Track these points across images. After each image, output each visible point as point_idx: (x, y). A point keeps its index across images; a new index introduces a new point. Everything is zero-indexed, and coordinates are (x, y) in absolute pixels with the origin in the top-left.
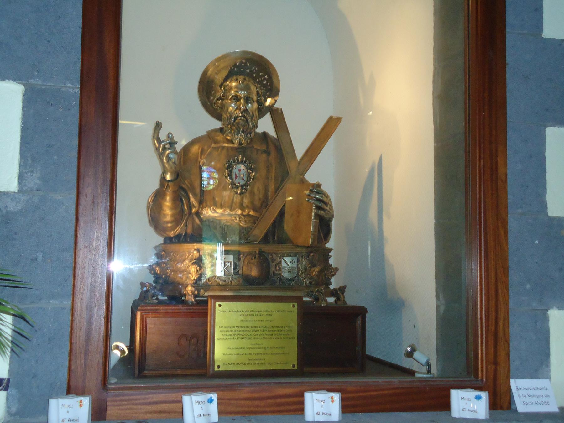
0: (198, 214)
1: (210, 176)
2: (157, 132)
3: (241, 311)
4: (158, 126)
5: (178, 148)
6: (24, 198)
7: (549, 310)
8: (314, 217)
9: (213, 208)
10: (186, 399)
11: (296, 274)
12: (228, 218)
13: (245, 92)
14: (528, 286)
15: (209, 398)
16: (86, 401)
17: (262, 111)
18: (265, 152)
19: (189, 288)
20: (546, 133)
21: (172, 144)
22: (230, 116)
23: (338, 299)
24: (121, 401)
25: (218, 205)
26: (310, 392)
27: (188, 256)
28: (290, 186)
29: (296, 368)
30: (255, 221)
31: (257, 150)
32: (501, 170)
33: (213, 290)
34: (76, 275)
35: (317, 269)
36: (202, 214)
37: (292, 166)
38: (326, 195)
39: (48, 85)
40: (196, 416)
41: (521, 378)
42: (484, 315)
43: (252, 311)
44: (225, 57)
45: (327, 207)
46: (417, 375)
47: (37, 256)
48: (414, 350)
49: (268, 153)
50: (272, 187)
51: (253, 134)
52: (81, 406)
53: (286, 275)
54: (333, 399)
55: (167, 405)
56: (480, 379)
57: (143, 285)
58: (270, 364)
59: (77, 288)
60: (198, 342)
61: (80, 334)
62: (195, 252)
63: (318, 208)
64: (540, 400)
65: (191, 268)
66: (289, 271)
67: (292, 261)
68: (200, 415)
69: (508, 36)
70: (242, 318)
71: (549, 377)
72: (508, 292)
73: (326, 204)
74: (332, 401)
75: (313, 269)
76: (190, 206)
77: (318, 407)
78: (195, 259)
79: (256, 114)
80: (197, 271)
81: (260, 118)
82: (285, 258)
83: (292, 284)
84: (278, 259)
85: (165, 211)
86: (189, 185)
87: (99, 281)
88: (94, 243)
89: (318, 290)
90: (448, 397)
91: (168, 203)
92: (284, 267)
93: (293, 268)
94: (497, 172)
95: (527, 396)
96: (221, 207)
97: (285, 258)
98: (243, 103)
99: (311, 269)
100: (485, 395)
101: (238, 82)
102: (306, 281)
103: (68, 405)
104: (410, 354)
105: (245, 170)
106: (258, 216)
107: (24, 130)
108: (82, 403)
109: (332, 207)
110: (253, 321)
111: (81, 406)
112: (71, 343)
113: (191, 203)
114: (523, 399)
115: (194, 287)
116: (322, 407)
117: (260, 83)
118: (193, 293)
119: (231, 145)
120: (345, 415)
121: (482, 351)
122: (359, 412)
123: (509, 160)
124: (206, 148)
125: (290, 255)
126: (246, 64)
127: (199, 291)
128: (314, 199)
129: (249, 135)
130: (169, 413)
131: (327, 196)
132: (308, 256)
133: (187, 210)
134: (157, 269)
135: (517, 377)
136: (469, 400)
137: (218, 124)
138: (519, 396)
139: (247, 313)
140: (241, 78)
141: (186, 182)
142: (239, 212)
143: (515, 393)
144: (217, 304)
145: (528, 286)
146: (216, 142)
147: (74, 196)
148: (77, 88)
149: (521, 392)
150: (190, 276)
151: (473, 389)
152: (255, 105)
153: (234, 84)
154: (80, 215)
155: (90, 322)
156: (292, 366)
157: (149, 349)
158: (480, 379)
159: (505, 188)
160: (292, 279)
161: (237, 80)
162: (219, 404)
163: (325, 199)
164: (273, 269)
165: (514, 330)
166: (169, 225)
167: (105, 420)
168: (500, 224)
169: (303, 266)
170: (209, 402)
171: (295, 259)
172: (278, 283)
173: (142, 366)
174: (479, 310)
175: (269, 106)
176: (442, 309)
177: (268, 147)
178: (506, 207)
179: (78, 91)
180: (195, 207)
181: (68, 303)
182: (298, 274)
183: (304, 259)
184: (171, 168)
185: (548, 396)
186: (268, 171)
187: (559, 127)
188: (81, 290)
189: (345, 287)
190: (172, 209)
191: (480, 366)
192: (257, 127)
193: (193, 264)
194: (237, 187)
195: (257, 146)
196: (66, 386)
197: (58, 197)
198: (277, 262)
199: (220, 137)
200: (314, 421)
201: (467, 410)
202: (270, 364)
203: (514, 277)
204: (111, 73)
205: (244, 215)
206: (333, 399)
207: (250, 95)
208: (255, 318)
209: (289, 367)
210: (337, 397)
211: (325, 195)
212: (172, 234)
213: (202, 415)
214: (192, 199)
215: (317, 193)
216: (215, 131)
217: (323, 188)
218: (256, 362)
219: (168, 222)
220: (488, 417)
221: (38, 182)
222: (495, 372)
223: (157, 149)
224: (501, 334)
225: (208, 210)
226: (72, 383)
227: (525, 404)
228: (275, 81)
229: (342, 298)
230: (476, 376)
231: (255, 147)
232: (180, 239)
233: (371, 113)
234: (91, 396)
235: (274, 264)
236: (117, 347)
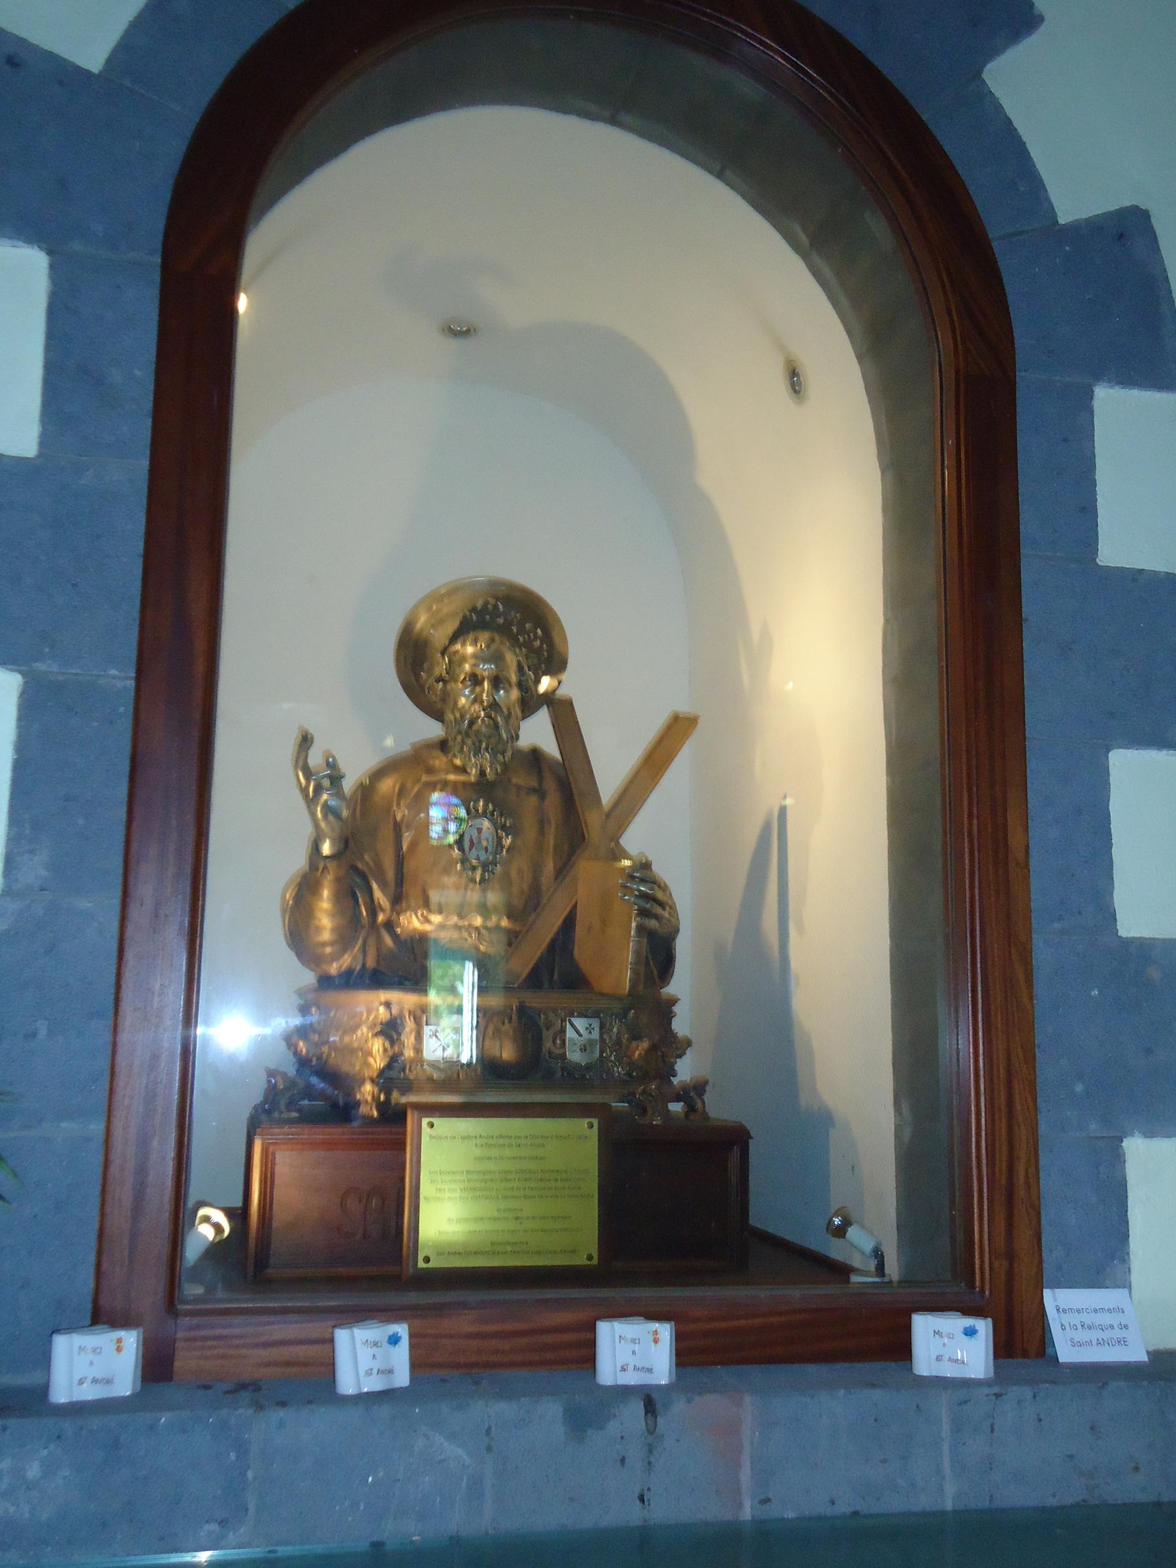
0: (389, 926)
1: (450, 814)
2: (303, 755)
3: (476, 1137)
4: (306, 741)
5: (348, 785)
6: (12, 906)
7: (1124, 1140)
8: (635, 932)
9: (422, 915)
10: (342, 1336)
11: (597, 1054)
12: (455, 935)
13: (493, 666)
14: (1079, 1088)
15: (391, 1333)
16: (131, 1339)
17: (530, 703)
18: (534, 791)
19: (368, 1088)
20: (1111, 763)
21: (336, 779)
22: (461, 716)
23: (691, 1108)
24: (205, 1338)
25: (433, 906)
26: (608, 1321)
27: (368, 1018)
28: (586, 868)
29: (595, 1261)
30: (513, 939)
31: (518, 787)
32: (1015, 838)
33: (420, 1090)
34: (117, 1069)
35: (645, 1044)
36: (399, 924)
37: (593, 821)
38: (663, 885)
39: (70, 673)
40: (362, 1373)
41: (1084, 1287)
42: (984, 1151)
43: (501, 1137)
44: (454, 590)
45: (664, 909)
46: (855, 1279)
47: (36, 1028)
48: (846, 1223)
49: (541, 793)
50: (549, 867)
51: (509, 754)
52: (119, 1350)
53: (575, 1056)
54: (657, 1336)
55: (304, 1347)
56: (977, 1289)
57: (271, 1073)
58: (539, 1253)
59: (117, 1098)
60: (383, 1203)
61: (123, 1194)
62: (382, 1009)
63: (643, 913)
64: (1106, 1335)
65: (372, 1045)
66: (584, 1049)
67: (588, 1026)
68: (369, 1371)
69: (1024, 563)
70: (478, 1152)
71: (1127, 1285)
72: (1035, 1101)
73: (662, 904)
74: (656, 1341)
75: (634, 1044)
76: (373, 909)
77: (624, 1355)
78: (381, 1023)
79: (517, 711)
80: (385, 1050)
81: (524, 718)
82: (573, 1020)
83: (590, 1077)
84: (560, 1021)
85: (320, 920)
86: (371, 863)
87: (163, 1082)
88: (156, 1000)
89: (644, 1088)
90: (907, 1329)
91: (325, 901)
92: (571, 1039)
93: (591, 1043)
94: (1006, 845)
95: (1079, 1326)
96: (440, 912)
97: (573, 1020)
98: (488, 689)
99: (630, 1043)
100: (984, 1326)
101: (479, 646)
102: (619, 1071)
103: (93, 1348)
104: (840, 1232)
105: (492, 830)
106: (518, 929)
107: (19, 767)
108: (122, 1344)
109: (676, 911)
110: (501, 1158)
111: (119, 1350)
112: (103, 1214)
113: (376, 902)
114: (1070, 1333)
115: (377, 1084)
116: (634, 1353)
117: (528, 645)
118: (375, 1099)
119: (462, 778)
120: (1001, 1361)
121: (980, 1230)
122: (716, 1364)
123: (1033, 818)
124: (409, 784)
125: (584, 1012)
126: (496, 607)
127: (388, 1094)
128: (637, 893)
129: (500, 757)
130: (306, 1364)
131: (664, 888)
132: (625, 1017)
133: (366, 918)
134: (301, 1044)
135: (1057, 1285)
136: (951, 1337)
137: (433, 730)
138: (1063, 1327)
139: (491, 1141)
140: (484, 637)
141: (366, 857)
142: (478, 921)
143: (1054, 1319)
144: (425, 1121)
145: (1079, 1088)
146: (430, 770)
147: (116, 902)
148: (131, 678)
149: (1067, 1319)
150: (371, 1060)
151: (959, 1313)
152: (515, 694)
153: (470, 650)
154: (127, 942)
155: (141, 1171)
156: (585, 1256)
157: (280, 1216)
158: (977, 1289)
159: (1026, 878)
160: (589, 1067)
161: (475, 642)
162: (412, 1347)
163: (660, 895)
164: (548, 1044)
165: (1050, 1184)
166: (328, 950)
167: (171, 1379)
168: (1015, 956)
169: (614, 1037)
170: (390, 1344)
171: (596, 1024)
172: (559, 1074)
173: (262, 1259)
174: (974, 1139)
175: (546, 694)
176: (907, 1133)
177: (541, 780)
178: (1028, 919)
179: (131, 684)
180: (382, 910)
181: (97, 1128)
182: (601, 1055)
183: (616, 1022)
184: (333, 830)
185: (1126, 1327)
186: (542, 831)
187: (1137, 750)
188: (127, 1101)
189: (706, 1082)
190: (333, 915)
191: (977, 1262)
192: (517, 737)
193: (376, 1035)
194: (474, 869)
195: (521, 779)
196: (89, 1306)
197: (84, 904)
198: (557, 1029)
199: (439, 761)
200: (614, 1384)
201: (946, 1358)
202: (539, 1253)
203: (1047, 1070)
204: (200, 646)
205: (485, 928)
206: (657, 1336)
207: (503, 671)
208: (508, 1152)
209: (580, 1260)
210: (665, 1331)
211: (659, 886)
212: (334, 969)
213: (375, 1371)
214: (378, 894)
215: (643, 881)
216: (429, 746)
217: (655, 868)
218: (509, 1248)
219: (324, 944)
220: (991, 1374)
221: (44, 873)
222: (1010, 1275)
223: (304, 791)
224: (1021, 1193)
225: (411, 916)
226: (104, 1301)
227: (1074, 1344)
228: (557, 639)
229: (699, 1105)
230: (972, 1285)
231: (514, 781)
232: (351, 980)
233: (790, 685)
234: (141, 1330)
235: (551, 1033)
236: (207, 1219)
